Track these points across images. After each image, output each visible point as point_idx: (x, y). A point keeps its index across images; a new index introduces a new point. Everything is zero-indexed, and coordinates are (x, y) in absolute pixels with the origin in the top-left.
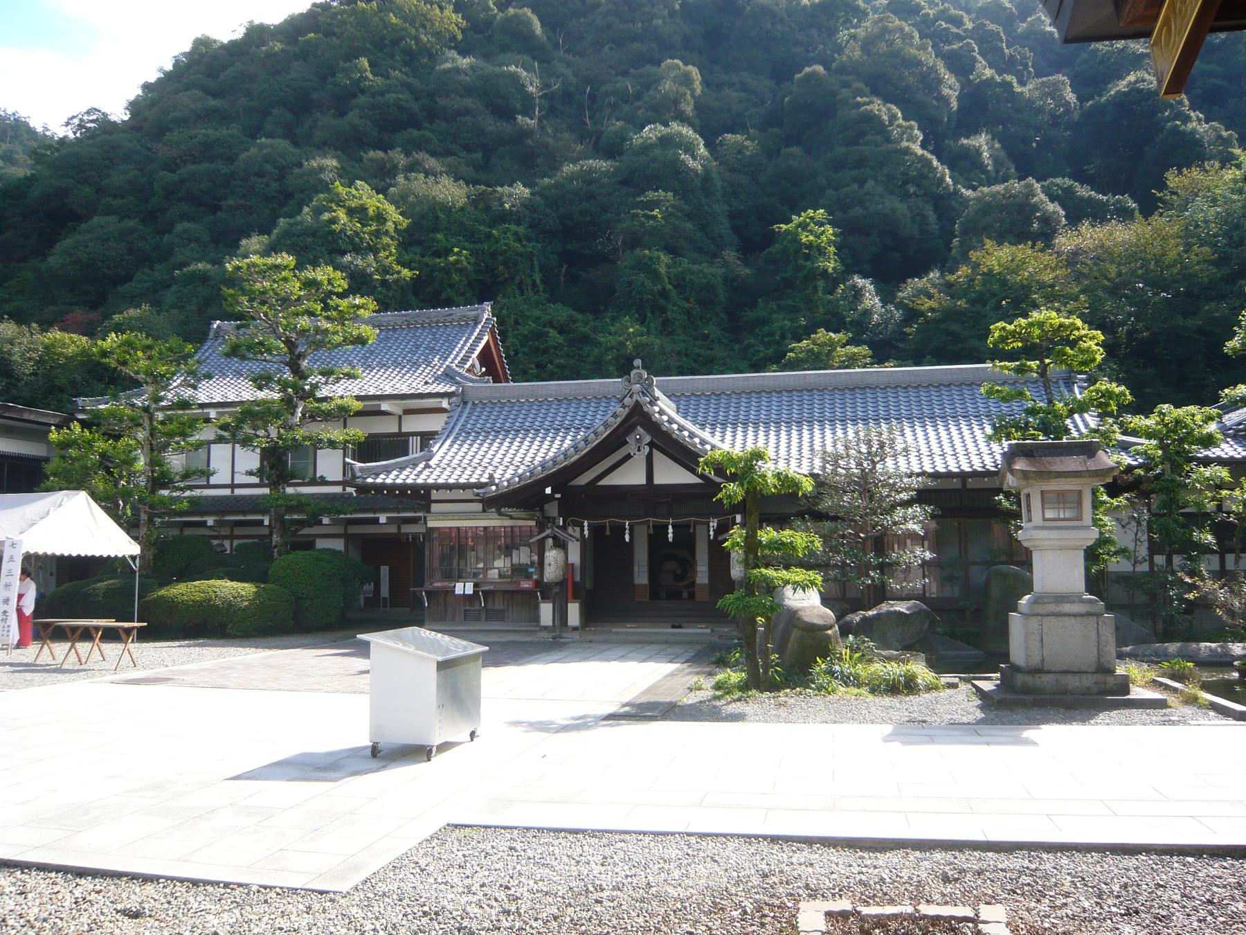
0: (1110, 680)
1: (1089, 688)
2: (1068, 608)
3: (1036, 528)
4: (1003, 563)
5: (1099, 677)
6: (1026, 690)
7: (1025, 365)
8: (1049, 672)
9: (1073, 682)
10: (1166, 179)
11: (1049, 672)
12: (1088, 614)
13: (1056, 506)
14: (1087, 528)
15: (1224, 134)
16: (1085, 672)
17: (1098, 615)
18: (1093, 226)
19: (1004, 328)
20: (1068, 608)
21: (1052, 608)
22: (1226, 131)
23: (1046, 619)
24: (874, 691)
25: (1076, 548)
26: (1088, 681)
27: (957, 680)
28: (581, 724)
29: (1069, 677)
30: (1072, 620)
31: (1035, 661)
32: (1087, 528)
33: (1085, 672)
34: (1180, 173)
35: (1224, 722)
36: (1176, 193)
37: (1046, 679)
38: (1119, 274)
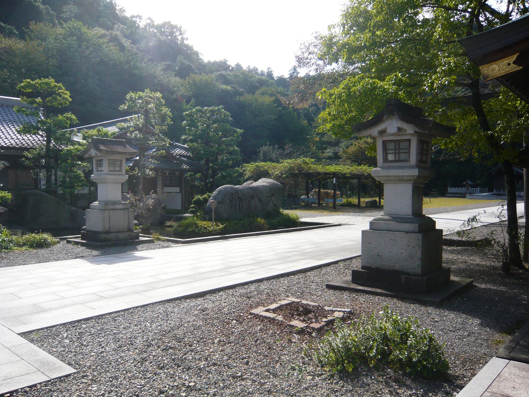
0: (133, 234)
1: (126, 238)
2: (117, 207)
3: (106, 174)
4: (34, 189)
5: (129, 233)
6: (105, 240)
7: (34, 100)
8: (112, 232)
9: (121, 236)
10: (30, 24)
11: (112, 232)
12: (124, 209)
13: (112, 165)
14: (124, 175)
15: (51, 12)
16: (124, 232)
17: (128, 209)
18: (5, 38)
19: (29, 82)
20: (117, 207)
21: (112, 207)
22: (52, 11)
23: (111, 211)
24: (31, 246)
25: (119, 183)
26: (126, 235)
27: (59, 240)
28: (345, 224)
29: (120, 234)
30: (120, 211)
31: (107, 228)
32: (124, 175)
33: (124, 232)
34: (36, 24)
35: (178, 245)
36: (33, 32)
37: (113, 235)
38: (20, 63)
